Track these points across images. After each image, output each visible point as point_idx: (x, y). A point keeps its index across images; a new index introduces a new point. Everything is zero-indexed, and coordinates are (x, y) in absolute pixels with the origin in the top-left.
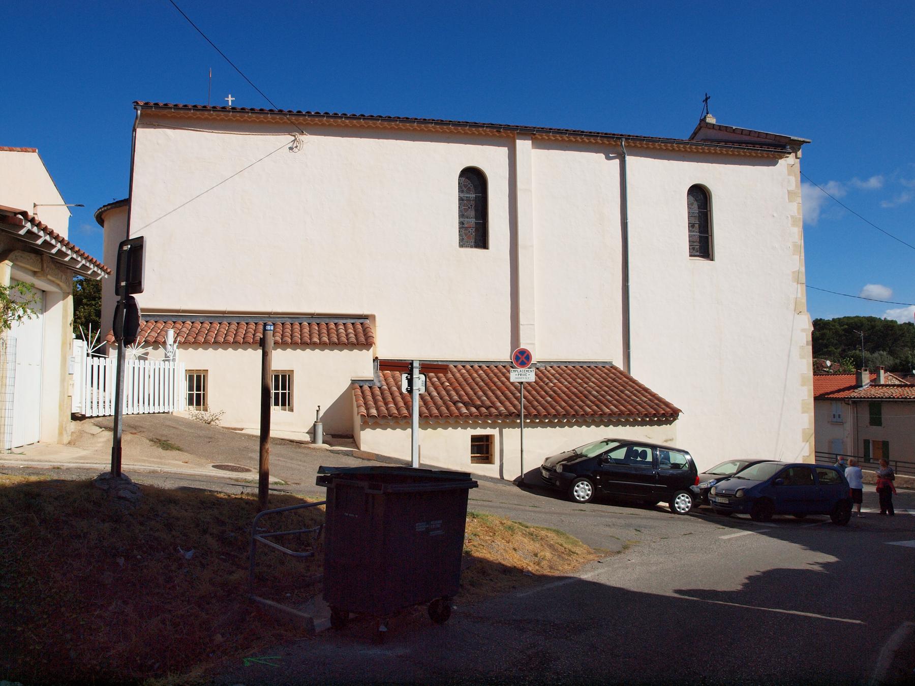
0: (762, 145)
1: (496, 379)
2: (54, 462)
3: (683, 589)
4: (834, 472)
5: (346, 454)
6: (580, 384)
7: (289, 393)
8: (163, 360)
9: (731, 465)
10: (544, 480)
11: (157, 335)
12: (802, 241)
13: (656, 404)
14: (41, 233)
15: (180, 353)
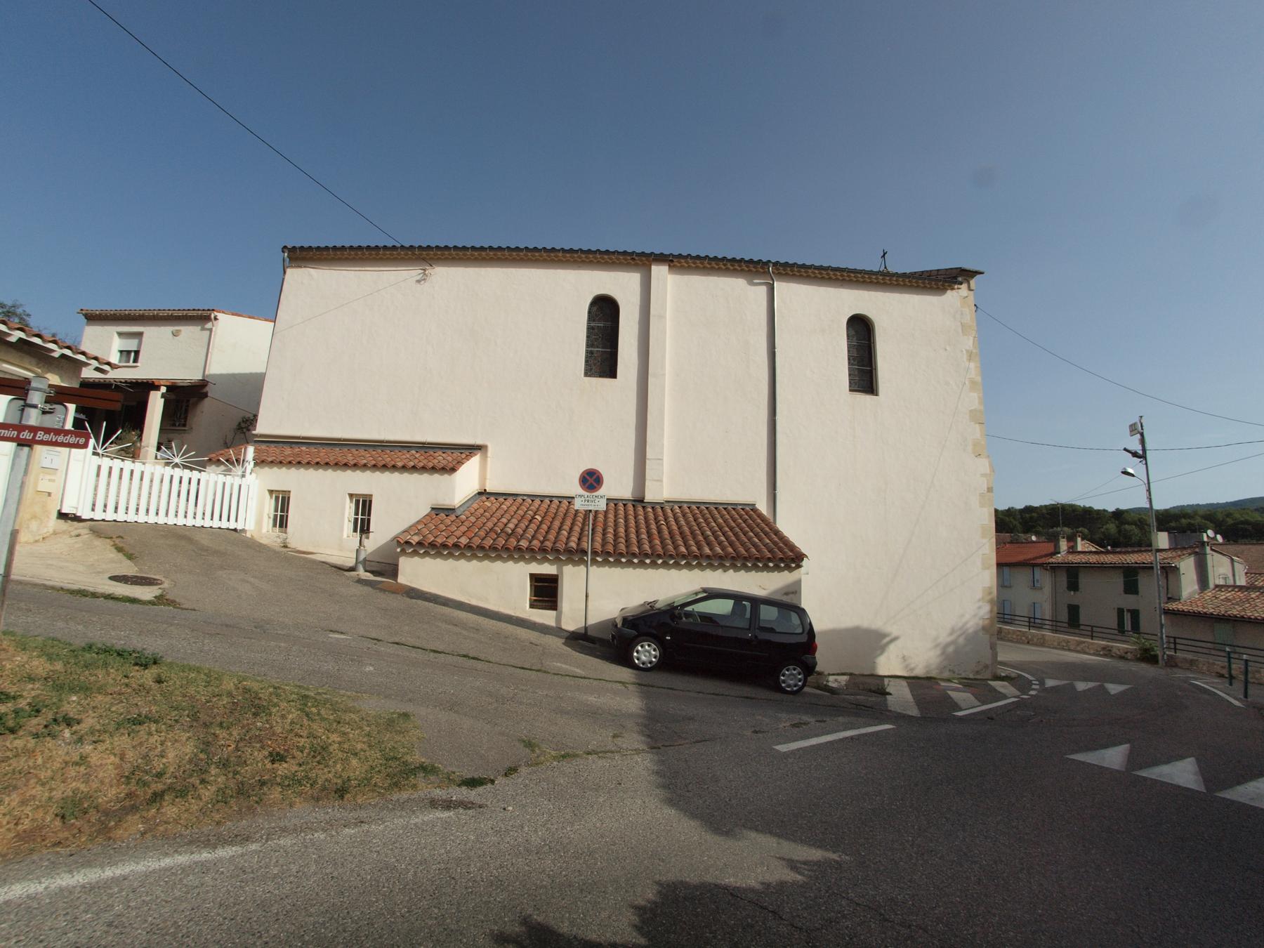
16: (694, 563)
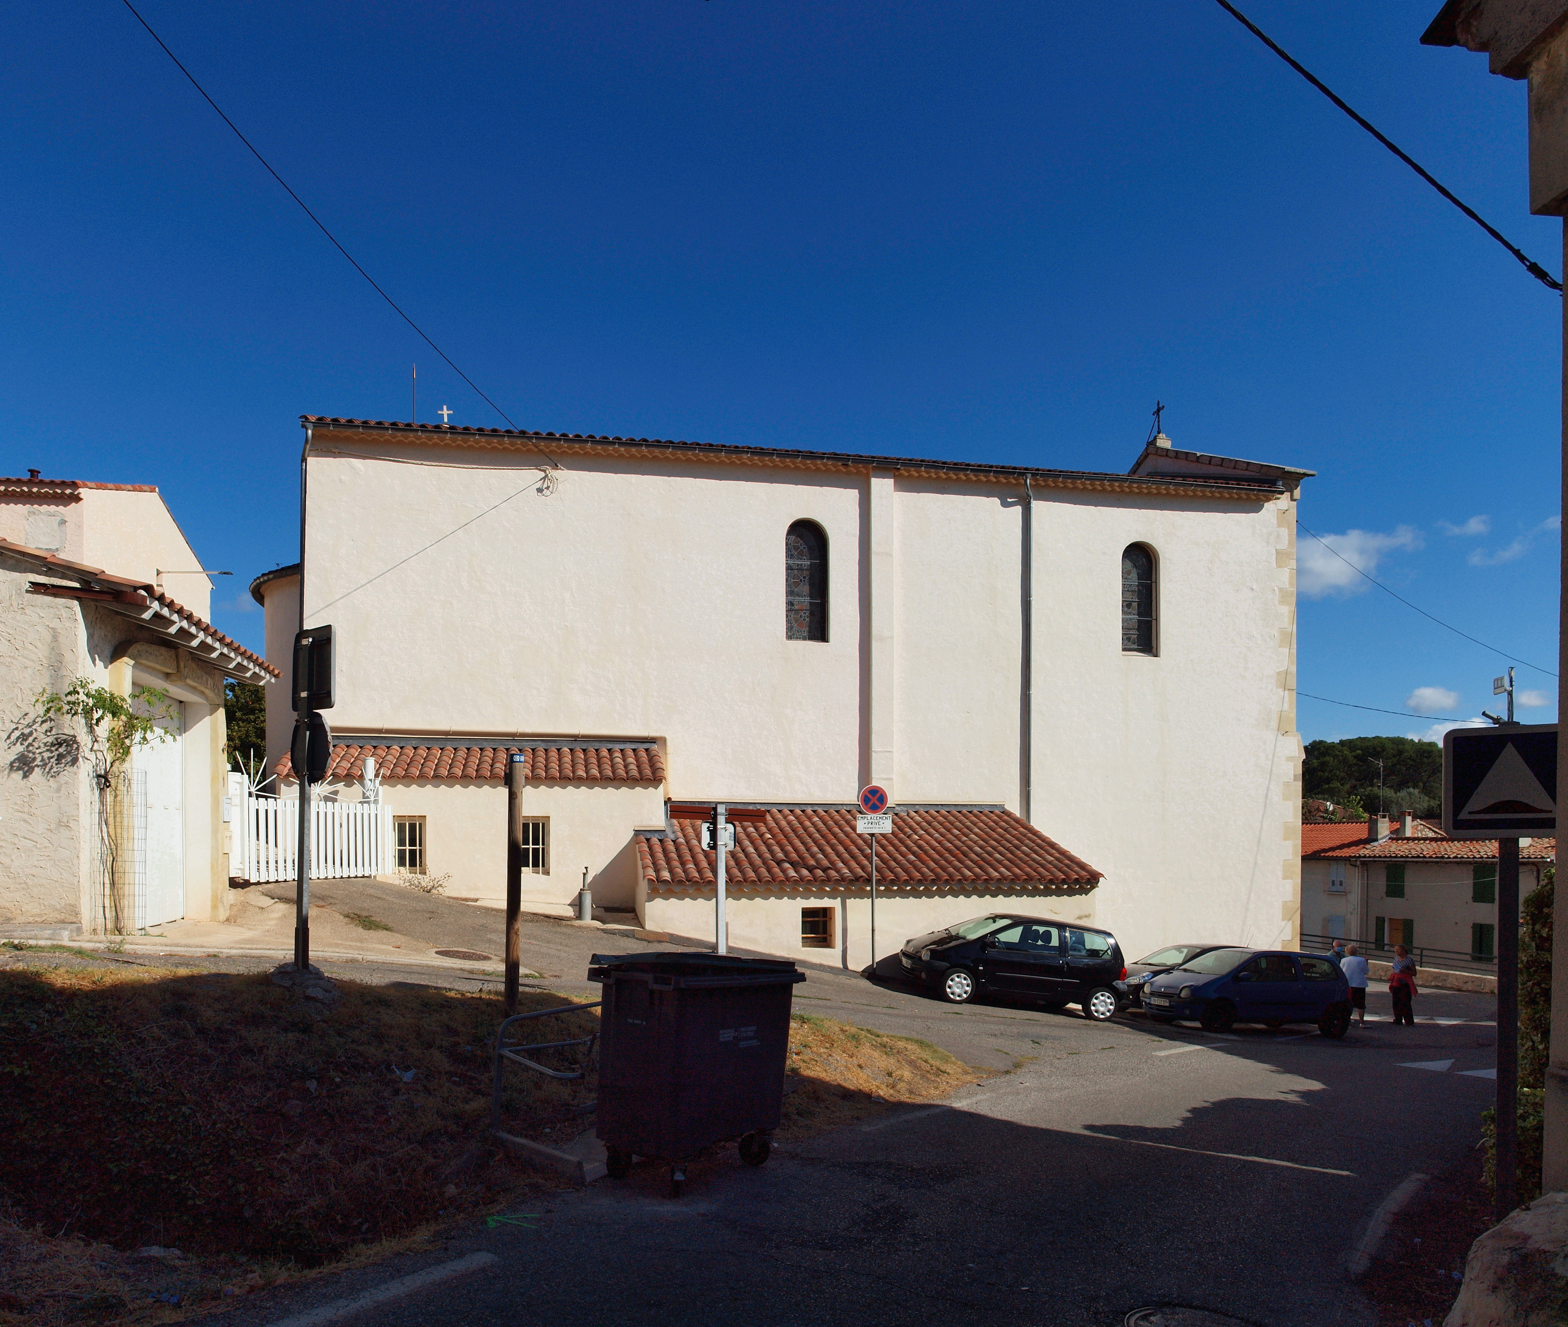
0: (1239, 480)
1: (837, 830)
2: (209, 947)
3: (1097, 1124)
4: (1326, 963)
5: (625, 934)
6: (956, 836)
7: (543, 849)
8: (360, 802)
9: (1174, 952)
10: (906, 971)
11: (349, 765)
12: (1295, 626)
13: (1068, 866)
14: (175, 617)
15: (384, 790)
16: (934, 889)
